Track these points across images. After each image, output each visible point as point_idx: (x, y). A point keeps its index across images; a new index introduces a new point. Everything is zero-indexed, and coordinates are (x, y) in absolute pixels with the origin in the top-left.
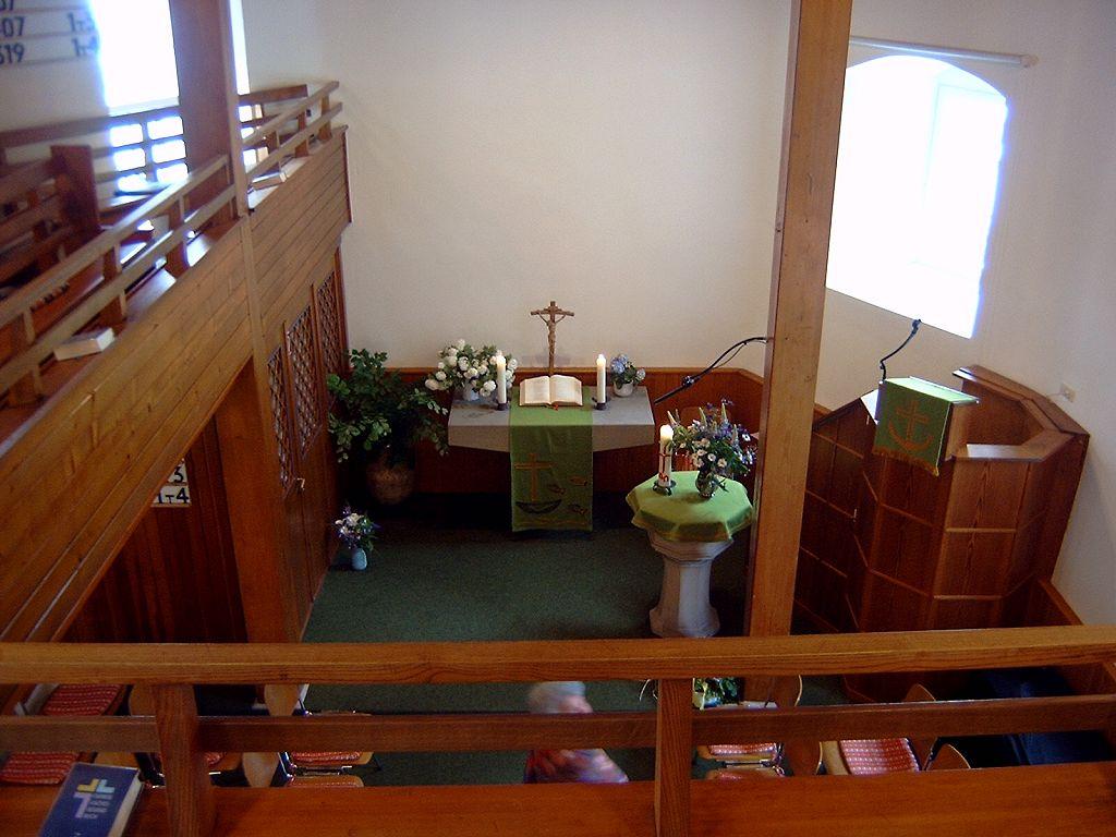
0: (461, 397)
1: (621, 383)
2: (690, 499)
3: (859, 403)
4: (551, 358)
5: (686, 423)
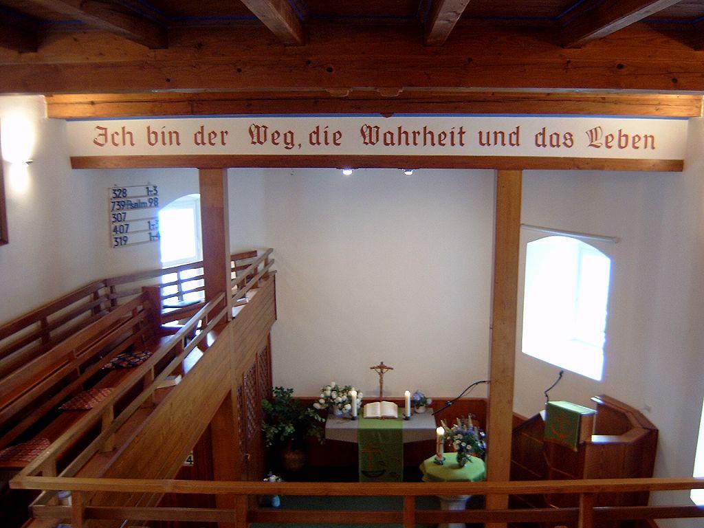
0: (332, 413)
2: (453, 467)
3: (539, 416)
4: (381, 393)
5: (450, 426)
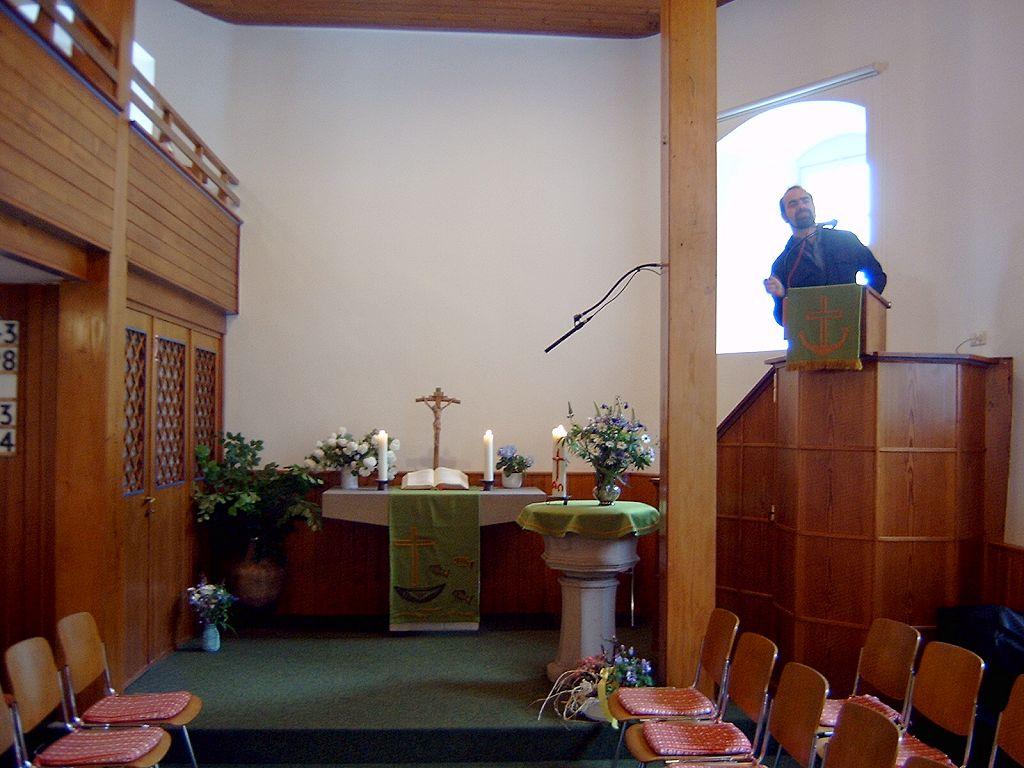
1: (510, 470)
